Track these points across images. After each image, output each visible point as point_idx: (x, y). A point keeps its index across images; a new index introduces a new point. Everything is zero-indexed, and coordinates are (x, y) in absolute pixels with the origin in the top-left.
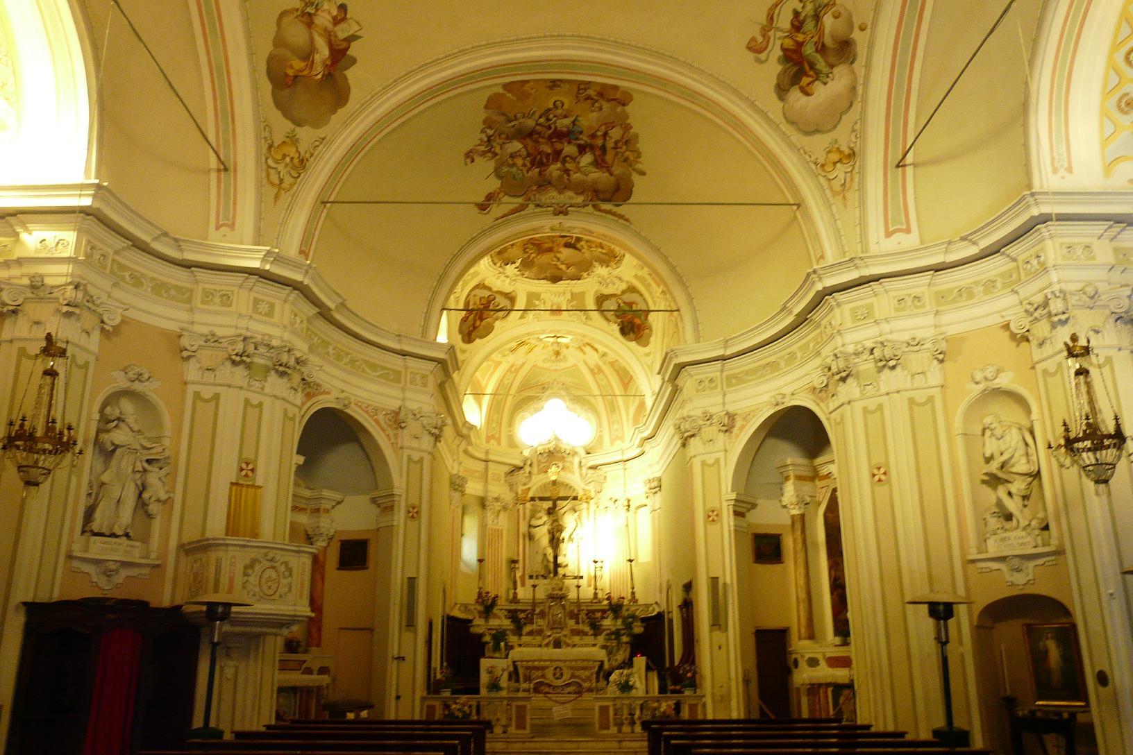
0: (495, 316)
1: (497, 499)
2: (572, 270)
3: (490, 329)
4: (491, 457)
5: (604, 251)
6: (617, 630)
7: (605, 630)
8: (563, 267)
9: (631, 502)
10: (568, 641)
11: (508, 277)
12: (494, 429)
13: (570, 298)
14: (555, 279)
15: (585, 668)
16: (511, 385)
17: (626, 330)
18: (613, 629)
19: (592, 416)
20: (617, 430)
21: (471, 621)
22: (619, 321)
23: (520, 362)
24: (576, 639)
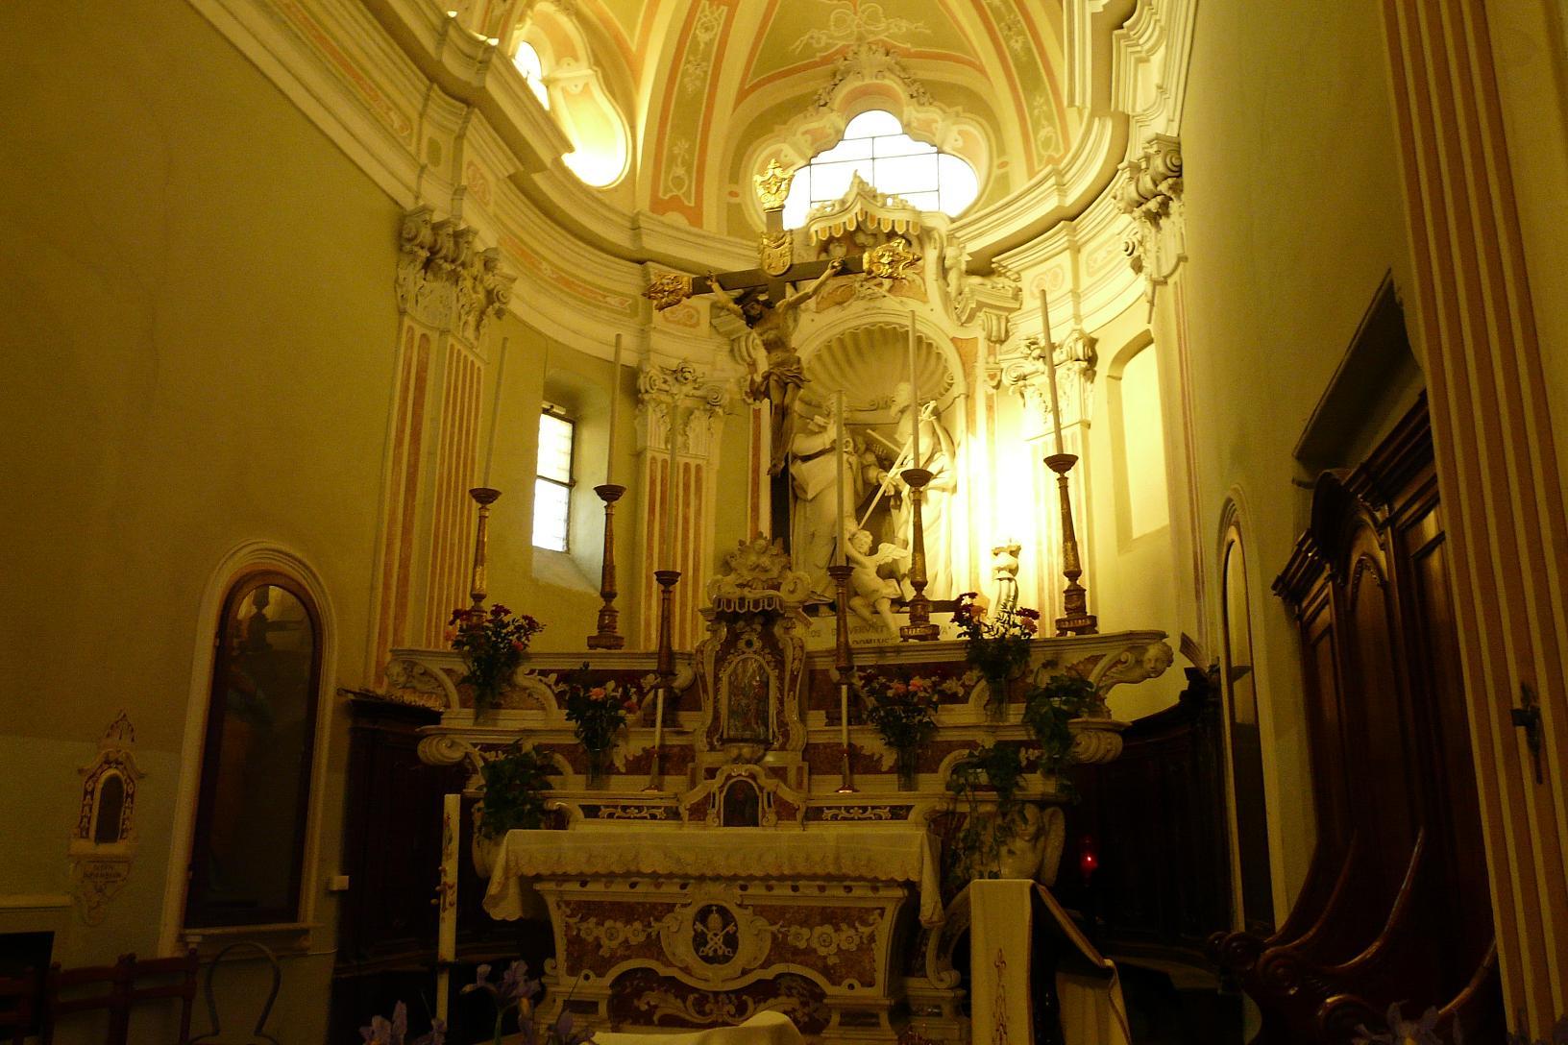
1: (679, 374)
4: (653, 244)
6: (1001, 745)
7: (950, 747)
9: (1098, 348)
10: (787, 794)
12: (678, 182)
15: (833, 917)
16: (723, 44)
18: (988, 742)
19: (974, 130)
20: (1047, 142)
21: (434, 717)
24: (829, 789)
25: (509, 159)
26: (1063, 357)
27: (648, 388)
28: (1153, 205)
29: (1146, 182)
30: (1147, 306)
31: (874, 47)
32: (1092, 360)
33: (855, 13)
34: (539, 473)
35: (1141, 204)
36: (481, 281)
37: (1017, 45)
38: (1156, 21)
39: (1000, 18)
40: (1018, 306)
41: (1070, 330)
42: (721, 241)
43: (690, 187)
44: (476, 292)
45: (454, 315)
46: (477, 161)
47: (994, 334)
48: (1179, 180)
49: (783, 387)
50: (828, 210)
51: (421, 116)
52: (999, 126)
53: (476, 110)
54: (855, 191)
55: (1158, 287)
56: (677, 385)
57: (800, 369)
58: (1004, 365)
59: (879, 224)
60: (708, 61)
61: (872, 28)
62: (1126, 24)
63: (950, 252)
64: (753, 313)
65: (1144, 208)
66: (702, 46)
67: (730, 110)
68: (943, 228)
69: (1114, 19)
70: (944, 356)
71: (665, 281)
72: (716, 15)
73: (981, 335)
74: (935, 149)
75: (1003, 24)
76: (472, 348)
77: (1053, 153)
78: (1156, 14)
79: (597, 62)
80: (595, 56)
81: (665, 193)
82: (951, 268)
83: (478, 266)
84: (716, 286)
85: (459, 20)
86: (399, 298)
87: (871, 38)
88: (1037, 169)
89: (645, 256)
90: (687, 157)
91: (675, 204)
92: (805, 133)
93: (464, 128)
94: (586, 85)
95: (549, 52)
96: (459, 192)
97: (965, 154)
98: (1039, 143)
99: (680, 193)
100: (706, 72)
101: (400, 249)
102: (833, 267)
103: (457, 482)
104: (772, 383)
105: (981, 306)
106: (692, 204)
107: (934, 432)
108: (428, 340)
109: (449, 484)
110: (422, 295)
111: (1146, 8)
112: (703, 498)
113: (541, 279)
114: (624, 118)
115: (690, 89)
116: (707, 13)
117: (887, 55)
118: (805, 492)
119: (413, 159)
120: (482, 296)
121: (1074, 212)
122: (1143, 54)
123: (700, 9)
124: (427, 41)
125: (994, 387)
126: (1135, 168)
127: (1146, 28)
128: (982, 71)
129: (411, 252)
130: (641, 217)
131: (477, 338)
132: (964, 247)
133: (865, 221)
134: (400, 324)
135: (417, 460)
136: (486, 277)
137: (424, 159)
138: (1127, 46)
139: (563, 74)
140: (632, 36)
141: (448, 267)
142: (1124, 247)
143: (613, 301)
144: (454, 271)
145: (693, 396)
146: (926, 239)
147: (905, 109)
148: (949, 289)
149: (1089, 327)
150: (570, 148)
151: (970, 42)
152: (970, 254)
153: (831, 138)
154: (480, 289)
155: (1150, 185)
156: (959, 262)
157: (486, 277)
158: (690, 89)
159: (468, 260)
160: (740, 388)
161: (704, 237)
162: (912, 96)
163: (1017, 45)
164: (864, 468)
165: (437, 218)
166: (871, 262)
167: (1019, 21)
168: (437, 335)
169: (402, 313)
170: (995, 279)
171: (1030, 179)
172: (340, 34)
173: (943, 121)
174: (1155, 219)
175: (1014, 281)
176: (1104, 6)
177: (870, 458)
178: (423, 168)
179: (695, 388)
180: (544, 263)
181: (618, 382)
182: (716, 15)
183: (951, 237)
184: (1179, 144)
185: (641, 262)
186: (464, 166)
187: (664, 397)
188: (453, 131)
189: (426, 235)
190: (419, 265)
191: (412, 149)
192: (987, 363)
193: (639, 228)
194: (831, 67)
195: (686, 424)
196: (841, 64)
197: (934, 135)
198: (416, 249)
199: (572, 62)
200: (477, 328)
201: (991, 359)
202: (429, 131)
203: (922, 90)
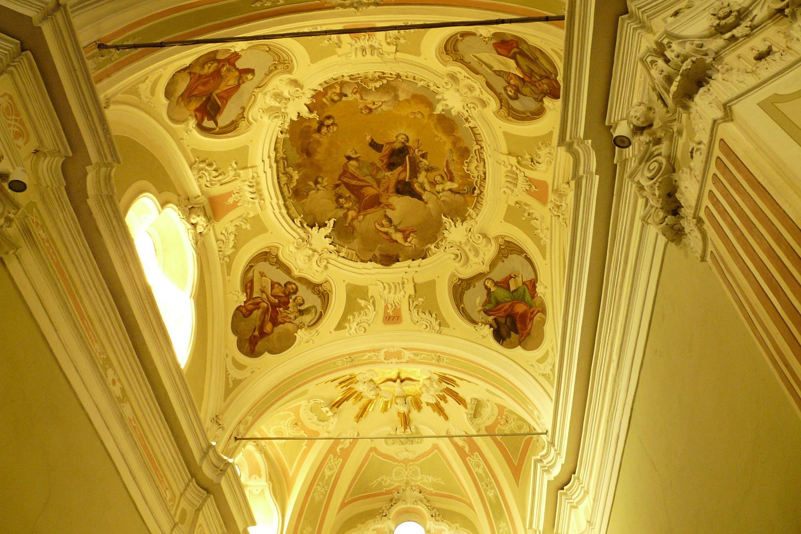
0: (297, 322)
2: (413, 240)
3: (287, 342)
5: (455, 186)
8: (398, 237)
11: (314, 251)
13: (412, 293)
14: (388, 260)
17: (503, 331)
22: (491, 319)
25: (221, 526)
31: (414, 488)
33: (406, 470)
37: (491, 494)
38: (582, 487)
39: (482, 480)
51: (181, 495)
53: (212, 496)
60: (328, 486)
61: (414, 478)
66: (327, 477)
67: (336, 513)
69: (559, 484)
75: (483, 483)
78: (582, 484)
79: (270, 479)
87: (413, 483)
92: (373, 530)
93: (202, 505)
94: (263, 491)
100: (326, 491)
111: (576, 481)
114: (279, 511)
115: (317, 499)
116: (332, 461)
117: (420, 493)
119: (172, 517)
122: (575, 504)
123: (328, 459)
127: (243, 532)
128: (471, 506)
137: (177, 520)
138: (565, 499)
150: (254, 523)
151: (464, 489)
158: (317, 499)
162: (432, 516)
163: (491, 494)
167: (492, 482)
172: (155, 447)
173: (449, 530)
178: (176, 525)
188: (196, 506)
194: (390, 496)
196: (396, 495)
202: (183, 504)
203: (437, 513)
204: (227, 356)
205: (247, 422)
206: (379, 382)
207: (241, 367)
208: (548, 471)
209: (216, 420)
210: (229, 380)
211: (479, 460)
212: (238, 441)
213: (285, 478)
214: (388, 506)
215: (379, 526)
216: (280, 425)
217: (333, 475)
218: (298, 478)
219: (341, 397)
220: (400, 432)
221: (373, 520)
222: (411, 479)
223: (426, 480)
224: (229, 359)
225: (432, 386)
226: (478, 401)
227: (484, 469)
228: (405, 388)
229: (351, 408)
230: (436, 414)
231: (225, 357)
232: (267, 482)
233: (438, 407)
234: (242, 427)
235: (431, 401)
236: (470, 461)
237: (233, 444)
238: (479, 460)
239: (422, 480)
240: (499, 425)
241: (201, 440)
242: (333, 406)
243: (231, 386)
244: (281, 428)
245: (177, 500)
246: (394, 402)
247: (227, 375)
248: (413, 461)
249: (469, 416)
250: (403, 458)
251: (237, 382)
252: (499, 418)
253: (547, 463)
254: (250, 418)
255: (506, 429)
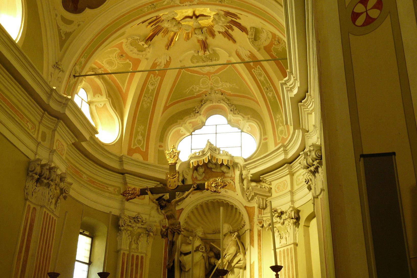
1: (136, 219)
4: (127, 167)
9: (300, 214)
12: (139, 142)
19: (255, 125)
20: (282, 132)
23: (162, 61)
25: (73, 138)
26: (287, 217)
27: (123, 224)
28: (312, 168)
29: (310, 160)
30: (312, 205)
31: (217, 92)
32: (298, 219)
34: (77, 259)
35: (308, 168)
36: (59, 186)
39: (264, 85)
40: (270, 195)
41: (289, 207)
42: (156, 166)
43: (144, 143)
44: (56, 190)
45: (47, 200)
46: (61, 140)
47: (261, 206)
48: (321, 161)
49: (173, 234)
50: (197, 154)
51: (40, 123)
52: (264, 123)
54: (208, 147)
55: (315, 199)
56: (135, 224)
57: (180, 227)
58: (264, 219)
59: (217, 160)
61: (216, 85)
62: (303, 101)
63: (244, 172)
64: (163, 204)
65: (309, 169)
66: (150, 90)
68: (242, 163)
70: (242, 214)
71: (130, 189)
72: (156, 80)
73: (256, 206)
74: (240, 130)
75: (264, 87)
76: (53, 212)
77: (284, 136)
79: (109, 96)
80: (109, 94)
81: (133, 146)
82: (245, 179)
83: (58, 180)
84: (149, 193)
85: (57, 90)
86: (26, 194)
87: (216, 89)
88: (278, 142)
89: (124, 172)
90: (143, 132)
91: (137, 150)
93: (56, 128)
95: (91, 92)
96: (52, 151)
97: (251, 133)
98: (279, 132)
99: (140, 146)
100: (152, 100)
101: (28, 174)
102: (194, 187)
103: (42, 267)
104: (169, 232)
105: (256, 194)
106: (144, 150)
107: (237, 244)
108: (36, 210)
109: (39, 268)
110: (35, 192)
112: (144, 270)
113: (83, 181)
116: (153, 79)
118: (185, 268)
119: (35, 140)
120: (58, 191)
121: (290, 161)
123: (150, 78)
124: (44, 97)
125: (261, 227)
126: (306, 154)
128: (257, 102)
129: (32, 176)
130: (123, 157)
131: (55, 208)
132: (250, 171)
133: (212, 159)
134: (25, 204)
135: (27, 259)
136: (61, 184)
137: (39, 140)
139: (96, 99)
140: (123, 87)
141: (45, 181)
142: (304, 181)
143: (111, 189)
144: (48, 183)
145: (141, 228)
146: (235, 167)
147: (229, 115)
148: (244, 187)
149: (297, 205)
152: (251, 174)
153: (199, 125)
154: (58, 188)
155: (311, 161)
156: (248, 177)
157: (61, 184)
159: (54, 178)
160: (160, 224)
161: (148, 165)
162: (231, 110)
164: (209, 258)
165: (43, 162)
166: (208, 186)
168: (39, 207)
169: (26, 199)
170: (262, 183)
171: (275, 147)
174: (314, 173)
175: (269, 185)
176: (294, 95)
177: (212, 254)
179: (142, 225)
180: (84, 175)
181: (110, 223)
182: (156, 80)
183: (245, 167)
184: (321, 147)
185: (123, 174)
186: (55, 141)
187: (130, 228)
189: (38, 169)
190: (34, 181)
191: (35, 136)
192: (258, 217)
193: (123, 161)
195: (138, 239)
196: (205, 98)
197: (240, 125)
198: (34, 175)
199: (100, 95)
200: (56, 204)
201: (260, 216)
203: (235, 108)
204: (56, 15)
205: (81, 63)
206: (179, 19)
207: (69, 22)
208: (291, 90)
209: (56, 66)
210: (62, 34)
211: (261, 71)
212: (77, 78)
213: (121, 94)
214: (200, 106)
215: (193, 120)
216: (110, 57)
217: (155, 88)
218: (129, 95)
219: (152, 33)
220: (201, 54)
221: (189, 116)
222: (214, 86)
223: (224, 86)
224: (59, 18)
225: (220, 19)
226: (256, 29)
227: (264, 77)
228: (200, 22)
229: (161, 41)
230: (226, 39)
231: (55, 16)
232: (107, 98)
233: (228, 34)
234: (77, 68)
235: (221, 30)
236: (254, 72)
237: (73, 80)
238: (261, 71)
239: (222, 86)
240: (274, 45)
241: (45, 87)
242: (147, 40)
243: (64, 38)
244: (111, 60)
245: (37, 127)
246: (193, 32)
247: (59, 30)
248: (214, 73)
249: (251, 40)
250: (206, 72)
251: (68, 35)
252: (273, 40)
253: (290, 85)
254: (83, 60)
255: (279, 48)
